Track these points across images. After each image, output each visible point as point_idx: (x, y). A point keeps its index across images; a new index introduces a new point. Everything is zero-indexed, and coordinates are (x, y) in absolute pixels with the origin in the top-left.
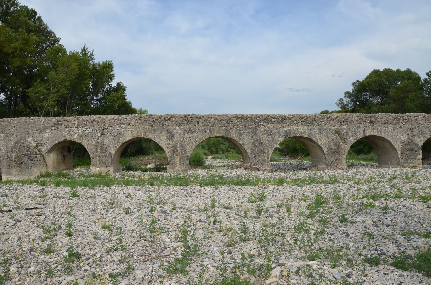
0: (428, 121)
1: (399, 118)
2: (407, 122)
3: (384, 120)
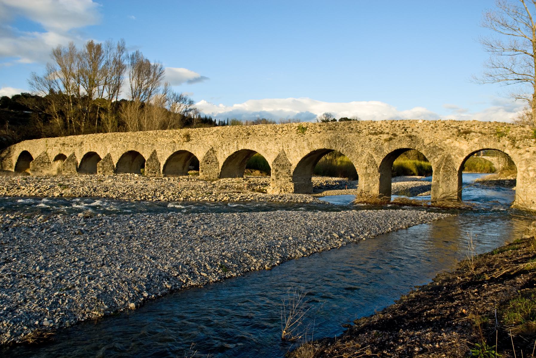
0: (311, 132)
1: (278, 129)
2: (287, 133)
3: (262, 132)
